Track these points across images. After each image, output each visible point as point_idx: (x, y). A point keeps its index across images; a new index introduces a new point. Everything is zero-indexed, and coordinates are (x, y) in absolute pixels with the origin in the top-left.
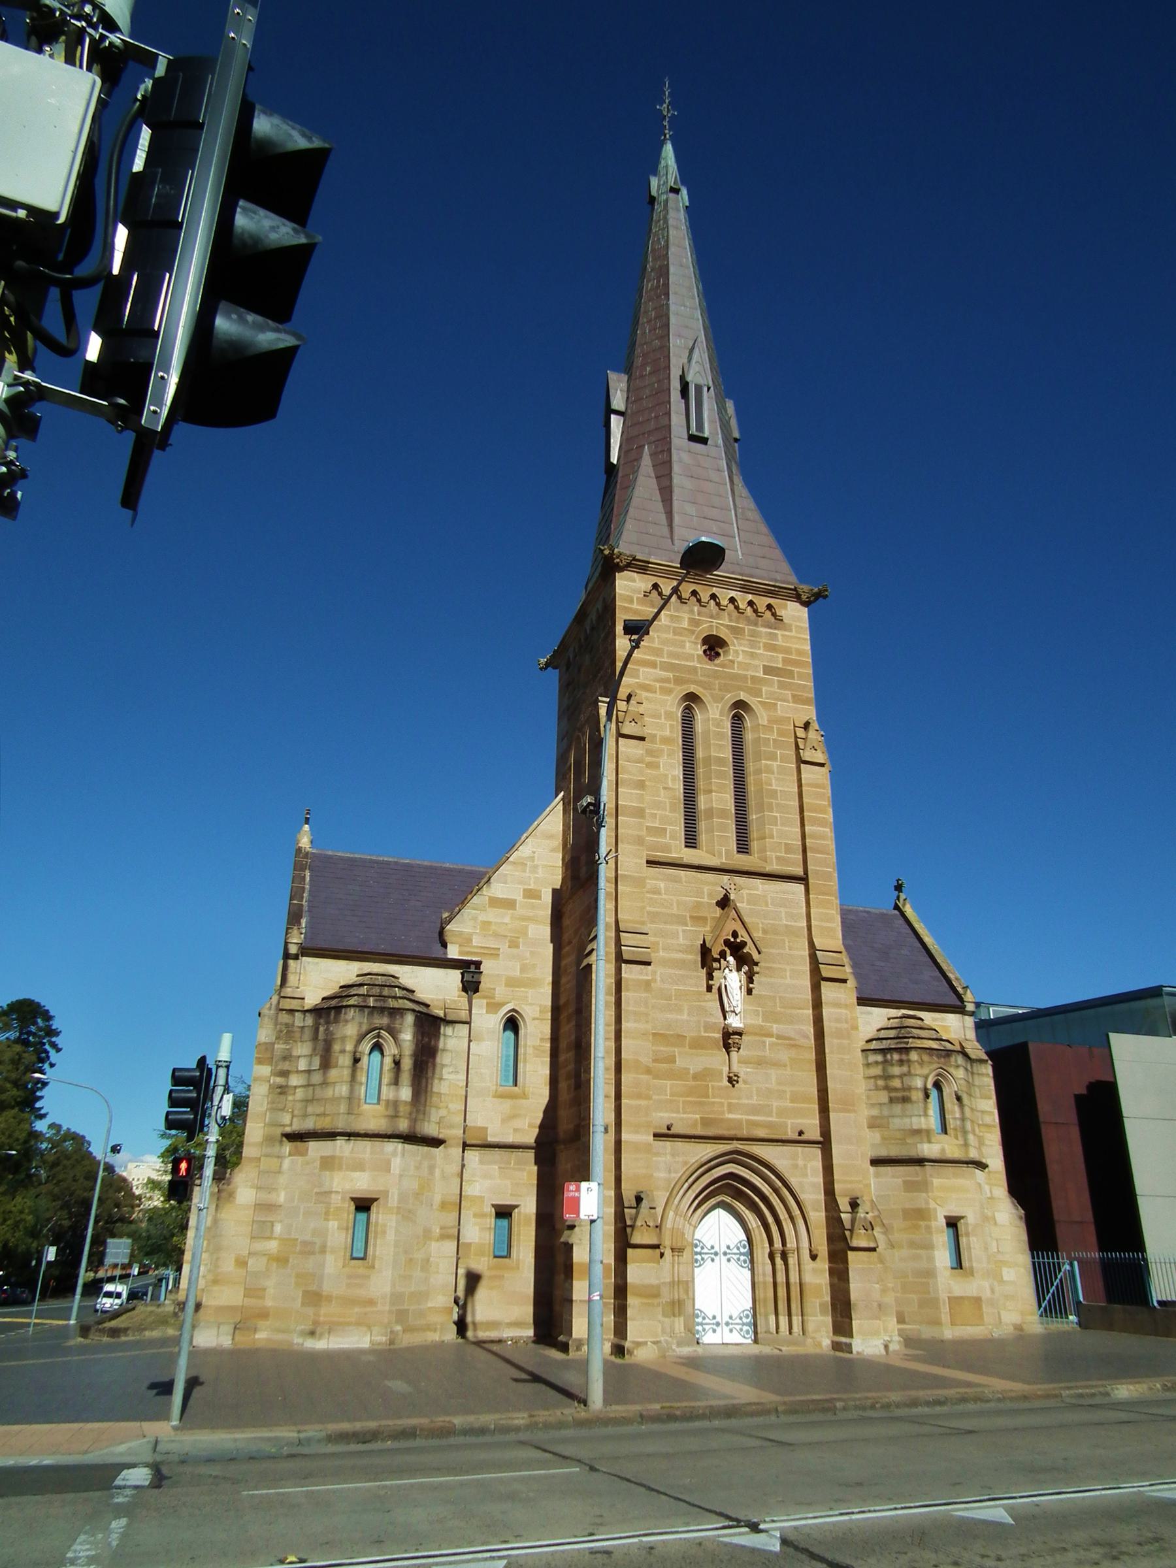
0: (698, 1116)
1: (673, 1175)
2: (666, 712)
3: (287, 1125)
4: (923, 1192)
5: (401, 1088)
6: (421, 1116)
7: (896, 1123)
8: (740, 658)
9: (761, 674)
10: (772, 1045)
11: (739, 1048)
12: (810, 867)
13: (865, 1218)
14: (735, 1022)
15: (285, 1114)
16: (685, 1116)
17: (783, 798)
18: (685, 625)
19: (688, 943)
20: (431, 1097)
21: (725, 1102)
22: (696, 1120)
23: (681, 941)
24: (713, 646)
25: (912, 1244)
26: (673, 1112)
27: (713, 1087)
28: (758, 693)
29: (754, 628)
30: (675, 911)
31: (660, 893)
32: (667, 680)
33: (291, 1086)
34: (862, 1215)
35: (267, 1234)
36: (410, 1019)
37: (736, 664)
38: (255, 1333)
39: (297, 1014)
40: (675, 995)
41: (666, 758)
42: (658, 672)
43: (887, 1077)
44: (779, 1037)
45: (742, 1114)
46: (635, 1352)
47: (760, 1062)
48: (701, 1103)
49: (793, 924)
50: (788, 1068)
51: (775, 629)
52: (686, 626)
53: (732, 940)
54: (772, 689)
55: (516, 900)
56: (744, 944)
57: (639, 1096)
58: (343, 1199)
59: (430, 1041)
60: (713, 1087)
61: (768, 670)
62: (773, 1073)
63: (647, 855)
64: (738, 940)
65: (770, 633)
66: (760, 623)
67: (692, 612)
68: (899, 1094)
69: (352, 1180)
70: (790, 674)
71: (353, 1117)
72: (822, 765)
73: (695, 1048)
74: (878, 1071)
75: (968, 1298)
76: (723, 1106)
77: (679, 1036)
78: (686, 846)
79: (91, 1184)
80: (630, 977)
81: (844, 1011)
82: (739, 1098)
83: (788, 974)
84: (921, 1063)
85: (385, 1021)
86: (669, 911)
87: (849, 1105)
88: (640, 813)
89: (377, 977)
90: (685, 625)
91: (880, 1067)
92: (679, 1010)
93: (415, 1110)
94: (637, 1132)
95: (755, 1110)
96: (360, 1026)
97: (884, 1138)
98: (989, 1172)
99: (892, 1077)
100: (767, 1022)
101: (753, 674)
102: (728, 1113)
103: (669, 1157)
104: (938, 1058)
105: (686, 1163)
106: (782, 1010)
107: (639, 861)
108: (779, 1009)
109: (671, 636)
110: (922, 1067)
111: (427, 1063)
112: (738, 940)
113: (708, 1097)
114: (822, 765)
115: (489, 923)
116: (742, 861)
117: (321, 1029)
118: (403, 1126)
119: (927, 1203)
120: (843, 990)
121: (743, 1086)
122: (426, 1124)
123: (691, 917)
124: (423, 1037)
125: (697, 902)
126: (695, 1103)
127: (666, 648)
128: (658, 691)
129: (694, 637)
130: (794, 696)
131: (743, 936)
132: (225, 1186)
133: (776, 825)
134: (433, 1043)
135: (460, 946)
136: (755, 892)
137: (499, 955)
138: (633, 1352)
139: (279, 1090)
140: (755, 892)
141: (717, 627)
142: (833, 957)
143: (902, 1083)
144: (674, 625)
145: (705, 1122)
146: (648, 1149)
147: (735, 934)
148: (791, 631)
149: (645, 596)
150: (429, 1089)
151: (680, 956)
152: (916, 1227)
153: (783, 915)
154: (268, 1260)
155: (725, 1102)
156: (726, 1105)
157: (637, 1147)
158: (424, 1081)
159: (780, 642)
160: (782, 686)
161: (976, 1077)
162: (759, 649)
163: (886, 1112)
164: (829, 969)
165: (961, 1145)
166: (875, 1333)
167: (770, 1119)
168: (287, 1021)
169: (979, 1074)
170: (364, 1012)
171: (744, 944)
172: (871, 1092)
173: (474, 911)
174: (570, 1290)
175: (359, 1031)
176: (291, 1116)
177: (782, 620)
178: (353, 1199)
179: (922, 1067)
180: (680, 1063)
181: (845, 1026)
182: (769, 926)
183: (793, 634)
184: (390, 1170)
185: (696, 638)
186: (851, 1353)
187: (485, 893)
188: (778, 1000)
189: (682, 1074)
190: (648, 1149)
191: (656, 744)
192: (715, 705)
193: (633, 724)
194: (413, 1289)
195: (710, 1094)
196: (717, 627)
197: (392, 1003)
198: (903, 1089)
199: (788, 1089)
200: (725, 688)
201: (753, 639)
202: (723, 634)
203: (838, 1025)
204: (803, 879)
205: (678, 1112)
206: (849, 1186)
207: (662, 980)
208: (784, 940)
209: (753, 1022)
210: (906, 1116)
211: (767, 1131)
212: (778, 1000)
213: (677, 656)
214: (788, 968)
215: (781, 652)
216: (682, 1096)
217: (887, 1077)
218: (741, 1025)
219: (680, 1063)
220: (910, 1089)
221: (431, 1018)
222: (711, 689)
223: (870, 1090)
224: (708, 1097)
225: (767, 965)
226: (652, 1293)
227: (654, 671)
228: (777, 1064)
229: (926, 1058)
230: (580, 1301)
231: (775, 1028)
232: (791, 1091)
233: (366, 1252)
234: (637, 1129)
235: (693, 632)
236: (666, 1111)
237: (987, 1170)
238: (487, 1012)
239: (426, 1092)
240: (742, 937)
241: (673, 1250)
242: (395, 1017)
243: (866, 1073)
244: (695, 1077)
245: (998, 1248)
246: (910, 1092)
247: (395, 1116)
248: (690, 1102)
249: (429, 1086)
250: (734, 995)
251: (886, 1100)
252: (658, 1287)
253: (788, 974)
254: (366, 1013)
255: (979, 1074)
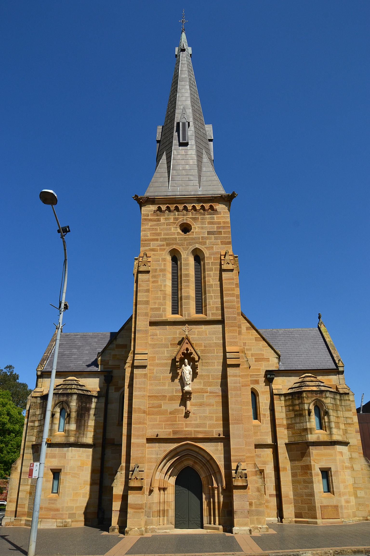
0: (171, 430)
1: (159, 456)
2: (162, 259)
3: (34, 441)
4: (308, 457)
5: (70, 425)
6: (82, 436)
7: (298, 426)
8: (197, 230)
9: (206, 235)
10: (207, 396)
11: (190, 399)
12: (225, 316)
13: (241, 472)
14: (187, 388)
15: (33, 437)
16: (165, 430)
17: (215, 287)
18: (172, 221)
19: (169, 355)
20: (87, 427)
21: (184, 423)
22: (170, 432)
23: (166, 355)
24: (186, 228)
25: (305, 482)
26: (160, 429)
27: (178, 417)
28: (205, 243)
29: (204, 216)
30: (164, 342)
31: (157, 335)
32: (163, 245)
33: (35, 426)
34: (240, 471)
35: (26, 484)
36: (75, 397)
37: (194, 233)
38: (21, 521)
39: (38, 398)
40: (163, 378)
41: (161, 278)
42: (159, 243)
43: (293, 405)
44: (210, 393)
45: (192, 428)
46: (129, 532)
47: (201, 405)
48: (172, 424)
49: (219, 342)
50: (215, 406)
51: (213, 215)
52: (172, 222)
53: (186, 352)
54: (211, 241)
55: (127, 344)
56: (191, 353)
57: (140, 423)
58: (48, 469)
59: (86, 405)
60: (178, 417)
61: (209, 233)
62: (207, 409)
63: (150, 320)
64: (189, 352)
65: (211, 217)
66: (206, 213)
67: (175, 215)
68: (298, 413)
69: (51, 462)
70: (220, 233)
71: (52, 437)
72: (232, 270)
73: (171, 401)
74: (289, 403)
75: (331, 506)
76: (183, 425)
77: (164, 396)
78: (172, 314)
79: (332, 442)
80: (138, 373)
81: (238, 378)
82: (191, 421)
83: (216, 364)
84: (307, 398)
85: (65, 398)
86: (161, 343)
87: (239, 421)
88: (147, 303)
89: (68, 381)
90: (172, 221)
91: (291, 401)
92: (164, 385)
93: (78, 433)
94: (138, 439)
95: (198, 426)
96: (55, 401)
97: (293, 434)
98: (350, 446)
99: (296, 405)
100: (205, 386)
101: (202, 236)
102: (186, 428)
103: (157, 448)
104: (316, 395)
105: (165, 451)
106: (213, 380)
107: (145, 323)
108: (211, 380)
109: (165, 227)
110: (307, 399)
111: (85, 414)
112: (189, 352)
113: (176, 421)
114: (232, 270)
115: (116, 355)
116: (177, 317)
117: (44, 403)
118: (72, 440)
119: (310, 462)
120: (238, 369)
121: (193, 415)
122: (84, 438)
123: (171, 344)
124: (82, 403)
125: (174, 337)
126: (170, 424)
127: (163, 232)
128: (159, 250)
129: (175, 225)
130: (221, 242)
131: (191, 350)
132: (14, 465)
133: (212, 299)
134: (88, 406)
135: (104, 366)
136: (201, 330)
137: (120, 368)
138: (128, 533)
139: (31, 428)
140: (201, 330)
141: (186, 219)
142: (234, 355)
143: (299, 407)
144: (167, 222)
145: (175, 432)
146: (143, 445)
147: (187, 349)
148: (221, 214)
149: (154, 212)
150: (86, 424)
151: (166, 361)
152: (306, 473)
153: (214, 338)
154: (26, 493)
155: (184, 423)
156: (184, 424)
157: (138, 445)
158: (83, 421)
159: (216, 220)
160: (216, 238)
161: (343, 401)
162: (206, 224)
163: (293, 422)
164: (231, 360)
165: (328, 434)
166: (246, 525)
167: (205, 429)
168: (34, 401)
169: (344, 400)
170: (57, 395)
171: (191, 353)
172: (288, 413)
173: (110, 351)
174: (276, 492)
175: (55, 403)
176: (35, 438)
177: (217, 211)
178: (51, 470)
179: (307, 399)
180: (164, 407)
181: (238, 385)
182: (207, 344)
183: (222, 215)
184: (65, 458)
185: (176, 225)
186: (232, 533)
187: (114, 343)
188: (211, 377)
189: (164, 413)
190: (143, 445)
191: (157, 273)
192: (185, 252)
193: (144, 266)
194: (78, 505)
195: (177, 420)
196: (186, 219)
197: (69, 391)
198: (300, 410)
199: (214, 415)
200: (190, 244)
201: (202, 221)
202: (189, 221)
203: (236, 385)
204: (222, 322)
205: (162, 429)
206: (238, 458)
207: (157, 373)
208: (214, 349)
209: (198, 387)
210: (301, 423)
211: (203, 435)
212: (211, 377)
213: (168, 234)
214: (216, 361)
215: (215, 224)
216: (163, 422)
217: (293, 405)
218: (191, 389)
219: (164, 407)
220: (302, 410)
221: (86, 396)
222: (182, 246)
223: (287, 412)
224: (176, 421)
225: (206, 361)
226: (139, 507)
227: (157, 242)
228: (209, 405)
229: (309, 395)
230: (116, 510)
231: (209, 389)
232: (216, 416)
233: (58, 491)
234: (138, 437)
235: (175, 223)
236: (157, 429)
237: (349, 445)
238: (115, 392)
239: (84, 426)
240: (190, 350)
241: (160, 489)
242: (69, 396)
243: (286, 404)
244: (171, 413)
245: (355, 481)
246: (302, 411)
247: (68, 436)
248: (167, 424)
249: (86, 423)
250: (187, 376)
251: (293, 416)
252: (142, 505)
253: (216, 364)
254: (58, 396)
255: (344, 400)
